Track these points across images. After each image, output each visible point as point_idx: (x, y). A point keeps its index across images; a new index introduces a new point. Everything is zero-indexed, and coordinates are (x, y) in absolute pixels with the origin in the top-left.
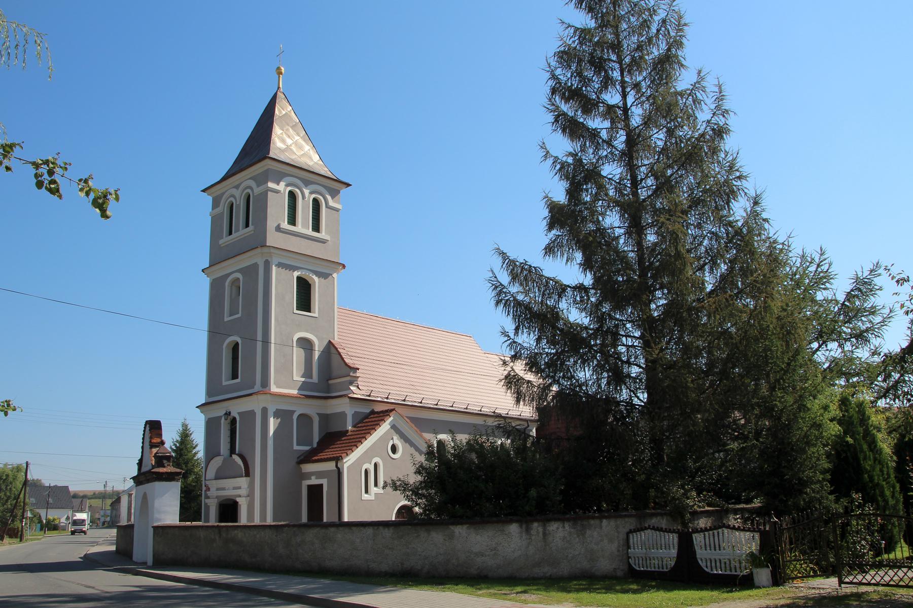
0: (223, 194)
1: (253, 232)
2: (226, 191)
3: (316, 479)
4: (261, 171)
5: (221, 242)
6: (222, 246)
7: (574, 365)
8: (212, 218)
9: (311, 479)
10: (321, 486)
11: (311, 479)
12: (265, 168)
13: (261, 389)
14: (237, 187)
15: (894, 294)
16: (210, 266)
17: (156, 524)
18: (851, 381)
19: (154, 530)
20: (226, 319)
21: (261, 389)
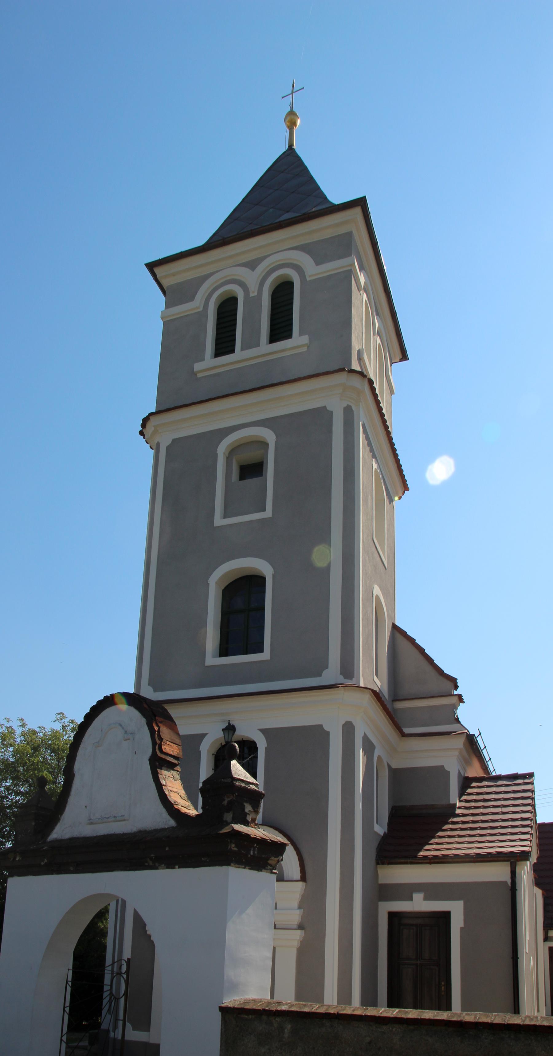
0: (204, 278)
1: (305, 349)
2: (269, 256)
3: (426, 898)
4: (328, 234)
5: (198, 367)
6: (199, 375)
7: (69, 737)
8: (166, 324)
9: (411, 899)
10: (445, 916)
11: (411, 899)
12: (342, 230)
13: (341, 679)
14: (252, 265)
15: (22, 720)
16: (158, 412)
17: (230, 1001)
18: (9, 792)
19: (225, 1022)
20: (219, 521)
21: (341, 679)
